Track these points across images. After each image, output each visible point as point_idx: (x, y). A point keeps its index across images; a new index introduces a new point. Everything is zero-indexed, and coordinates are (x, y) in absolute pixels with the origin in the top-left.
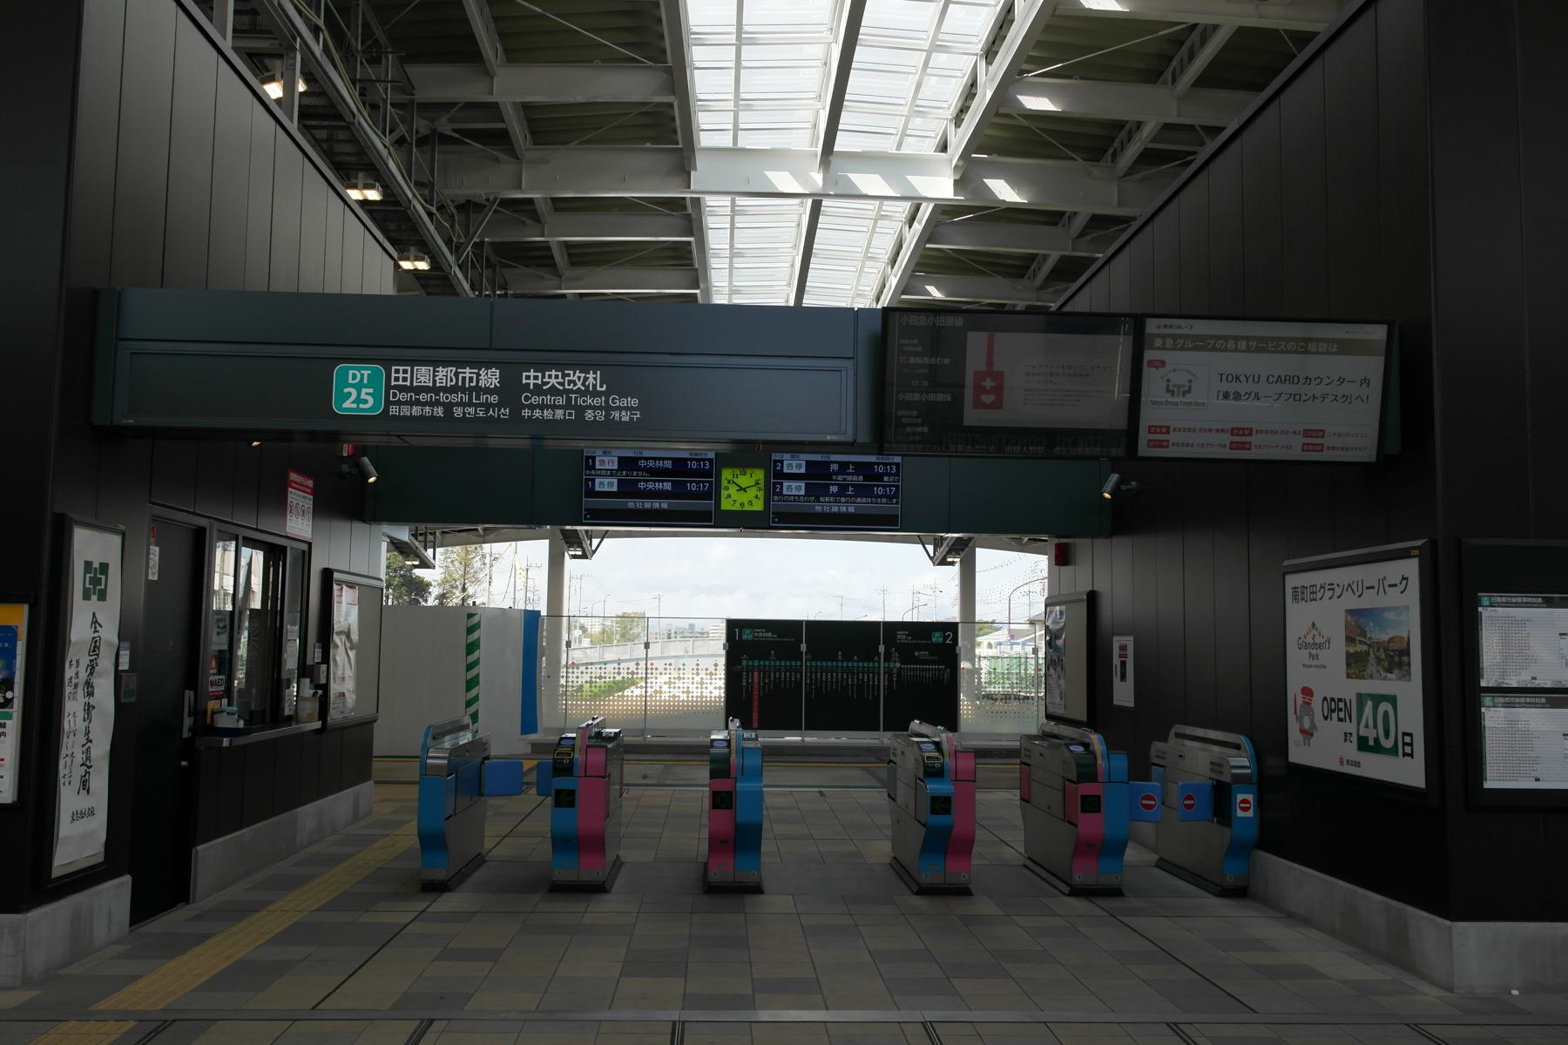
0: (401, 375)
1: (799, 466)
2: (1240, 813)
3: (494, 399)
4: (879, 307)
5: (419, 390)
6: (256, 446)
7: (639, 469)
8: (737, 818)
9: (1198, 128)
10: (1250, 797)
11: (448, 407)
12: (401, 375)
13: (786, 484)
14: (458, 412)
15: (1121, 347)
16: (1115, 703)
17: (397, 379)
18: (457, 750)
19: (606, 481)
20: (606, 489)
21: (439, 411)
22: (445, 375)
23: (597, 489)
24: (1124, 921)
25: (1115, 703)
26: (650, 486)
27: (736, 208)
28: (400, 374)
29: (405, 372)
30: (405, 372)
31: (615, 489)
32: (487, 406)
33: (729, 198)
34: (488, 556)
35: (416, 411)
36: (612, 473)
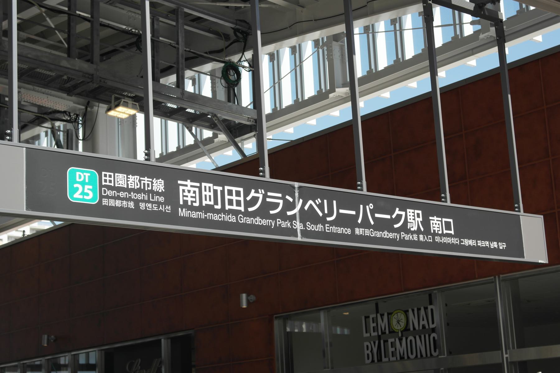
3: (162, 199)
5: (119, 189)
11: (137, 202)
14: (142, 206)
21: (131, 205)
32: (158, 203)
35: (118, 203)
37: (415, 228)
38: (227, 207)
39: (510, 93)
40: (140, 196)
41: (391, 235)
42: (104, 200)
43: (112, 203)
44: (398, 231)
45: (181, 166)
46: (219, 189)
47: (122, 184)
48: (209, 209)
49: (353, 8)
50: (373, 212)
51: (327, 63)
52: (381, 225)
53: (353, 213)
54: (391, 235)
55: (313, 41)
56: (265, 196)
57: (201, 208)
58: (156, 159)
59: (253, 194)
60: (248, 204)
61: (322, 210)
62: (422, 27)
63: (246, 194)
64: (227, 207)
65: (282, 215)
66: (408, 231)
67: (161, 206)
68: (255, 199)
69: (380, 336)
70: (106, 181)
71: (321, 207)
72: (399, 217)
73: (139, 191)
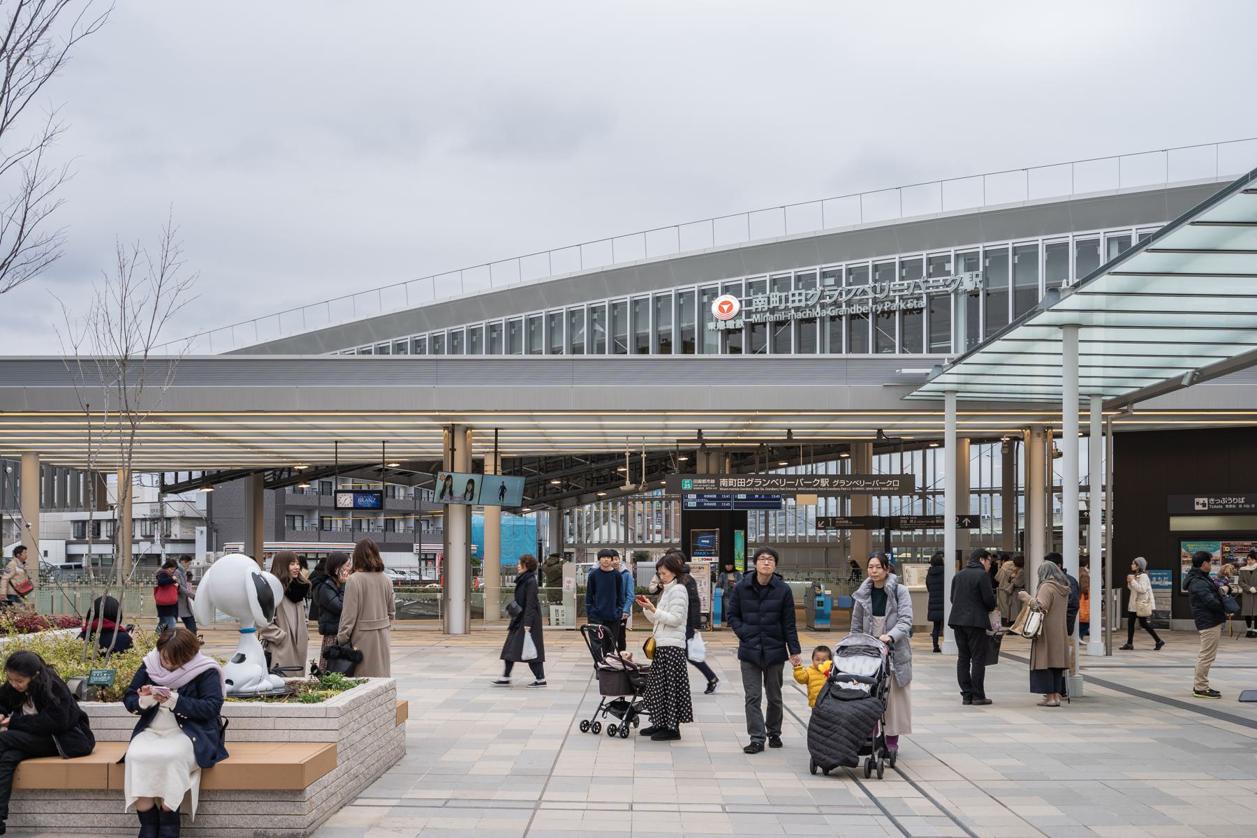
0: (741, 482)
1: (694, 504)
4: (1133, 562)
5: (699, 484)
7: (704, 498)
11: (705, 488)
12: (741, 482)
16: (1171, 529)
18: (672, 557)
19: (692, 503)
22: (704, 481)
25: (1171, 529)
26: (708, 504)
27: (866, 444)
28: (695, 481)
29: (740, 484)
30: (743, 481)
33: (998, 483)
34: (1069, 492)
36: (694, 500)
37: (824, 485)
40: (707, 485)
41: (814, 489)
42: (743, 481)
43: (697, 489)
44: (815, 487)
46: (735, 480)
47: (836, 275)
48: (732, 487)
49: (1134, 408)
50: (803, 482)
52: (881, 486)
54: (814, 489)
55: (483, 528)
56: (754, 481)
57: (728, 487)
59: (749, 480)
60: (746, 484)
62: (899, 454)
63: (746, 481)
65: (761, 486)
66: (821, 487)
67: (527, 629)
69: (986, 267)
70: (740, 481)
71: (778, 482)
73: (706, 484)
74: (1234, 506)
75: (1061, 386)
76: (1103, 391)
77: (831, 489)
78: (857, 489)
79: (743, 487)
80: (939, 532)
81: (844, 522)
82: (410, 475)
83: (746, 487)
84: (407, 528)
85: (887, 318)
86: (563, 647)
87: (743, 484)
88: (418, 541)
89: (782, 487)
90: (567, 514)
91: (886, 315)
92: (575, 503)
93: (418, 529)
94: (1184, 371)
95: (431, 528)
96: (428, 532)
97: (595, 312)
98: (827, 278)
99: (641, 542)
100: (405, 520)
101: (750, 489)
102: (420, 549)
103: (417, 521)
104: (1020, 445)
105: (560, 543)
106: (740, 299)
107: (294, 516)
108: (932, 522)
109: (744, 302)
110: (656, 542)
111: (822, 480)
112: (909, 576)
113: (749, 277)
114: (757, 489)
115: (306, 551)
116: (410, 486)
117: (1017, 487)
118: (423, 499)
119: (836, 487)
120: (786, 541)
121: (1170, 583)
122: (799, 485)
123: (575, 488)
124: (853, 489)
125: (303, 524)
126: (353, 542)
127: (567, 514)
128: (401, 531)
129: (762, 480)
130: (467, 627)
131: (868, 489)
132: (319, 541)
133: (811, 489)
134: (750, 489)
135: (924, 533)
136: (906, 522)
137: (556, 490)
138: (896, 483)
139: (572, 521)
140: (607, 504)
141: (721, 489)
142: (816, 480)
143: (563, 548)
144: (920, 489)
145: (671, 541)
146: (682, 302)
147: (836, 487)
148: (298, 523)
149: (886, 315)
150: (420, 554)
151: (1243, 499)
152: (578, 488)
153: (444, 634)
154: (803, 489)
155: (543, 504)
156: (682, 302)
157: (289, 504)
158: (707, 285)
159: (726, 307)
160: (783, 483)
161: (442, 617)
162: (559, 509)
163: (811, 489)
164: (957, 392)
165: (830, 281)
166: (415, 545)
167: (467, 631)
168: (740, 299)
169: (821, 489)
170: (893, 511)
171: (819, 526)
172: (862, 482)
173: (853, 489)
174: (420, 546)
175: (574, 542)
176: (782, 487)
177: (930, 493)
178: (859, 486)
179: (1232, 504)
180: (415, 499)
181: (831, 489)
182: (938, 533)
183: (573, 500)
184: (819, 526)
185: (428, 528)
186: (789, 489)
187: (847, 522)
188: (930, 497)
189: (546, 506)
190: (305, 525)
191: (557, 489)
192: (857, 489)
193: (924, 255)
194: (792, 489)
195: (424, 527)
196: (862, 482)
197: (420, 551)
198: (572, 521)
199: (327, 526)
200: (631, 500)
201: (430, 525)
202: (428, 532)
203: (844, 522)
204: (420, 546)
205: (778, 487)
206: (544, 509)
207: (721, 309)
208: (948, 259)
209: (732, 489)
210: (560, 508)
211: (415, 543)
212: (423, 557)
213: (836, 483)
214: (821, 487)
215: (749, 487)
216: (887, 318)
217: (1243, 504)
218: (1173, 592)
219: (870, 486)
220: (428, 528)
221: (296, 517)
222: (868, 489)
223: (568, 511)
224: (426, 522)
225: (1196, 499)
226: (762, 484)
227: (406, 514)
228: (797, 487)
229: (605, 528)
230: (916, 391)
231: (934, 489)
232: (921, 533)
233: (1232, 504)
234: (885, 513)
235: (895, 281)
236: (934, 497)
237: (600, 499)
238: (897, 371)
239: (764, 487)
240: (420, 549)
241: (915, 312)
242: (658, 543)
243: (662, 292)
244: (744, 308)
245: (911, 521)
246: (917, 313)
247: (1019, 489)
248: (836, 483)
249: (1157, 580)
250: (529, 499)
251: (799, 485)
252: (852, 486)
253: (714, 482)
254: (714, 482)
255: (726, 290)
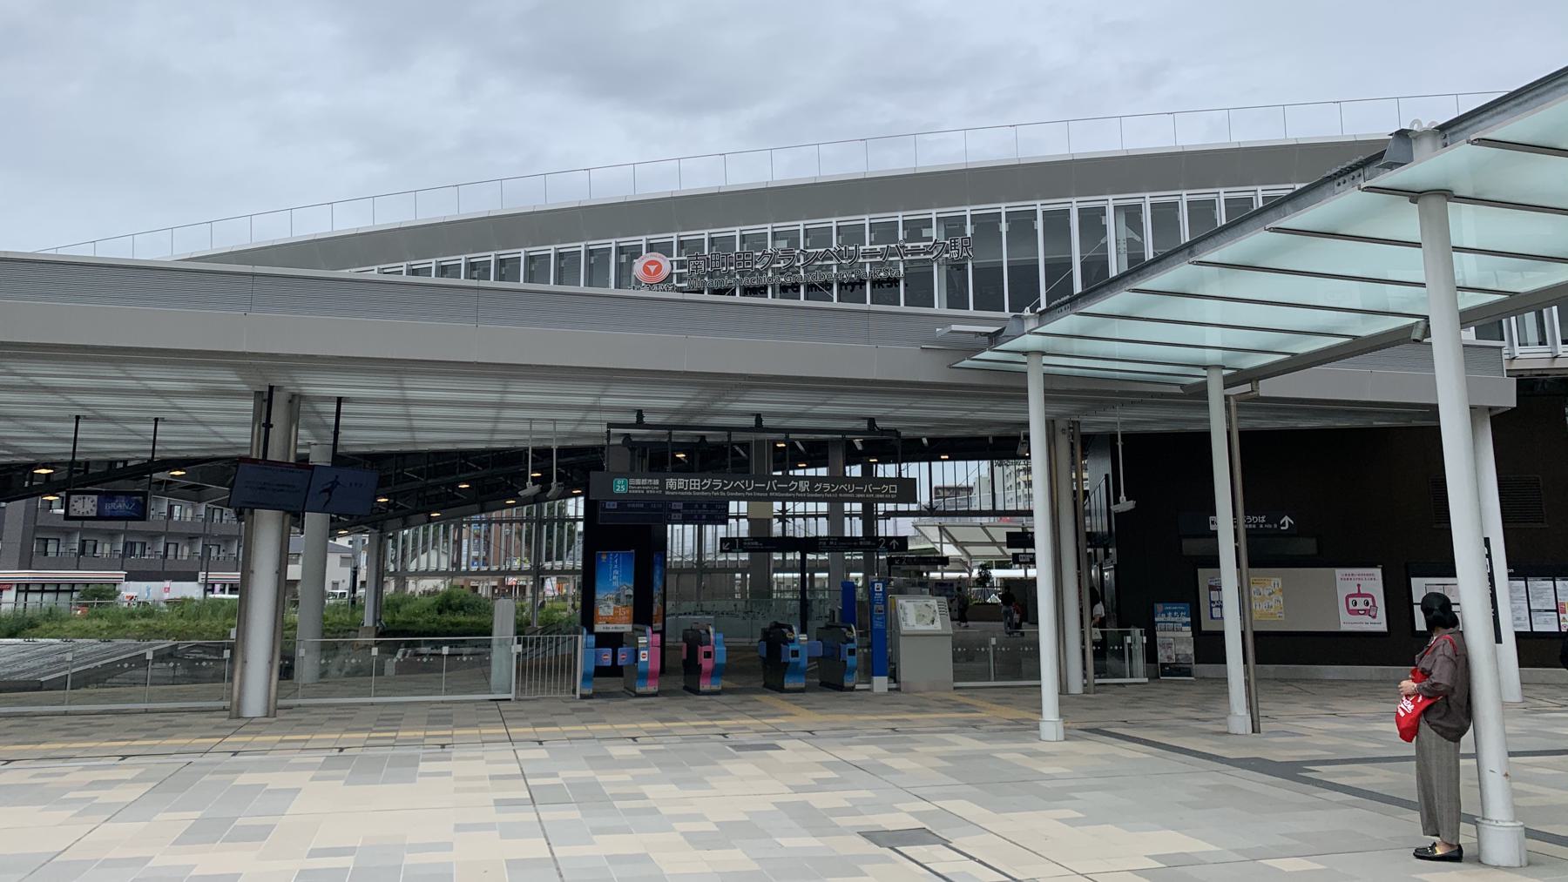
0: (695, 484)
2: (642, 659)
3: (657, 488)
5: (637, 486)
6: (24, 483)
8: (1516, 865)
9: (633, 278)
10: (642, 659)
11: (645, 490)
12: (695, 484)
13: (673, 515)
14: (648, 492)
15: (840, 436)
17: (693, 486)
20: (611, 507)
21: (643, 492)
22: (644, 481)
23: (607, 507)
24: (1004, 877)
28: (632, 481)
29: (697, 482)
30: (697, 482)
31: (616, 507)
32: (655, 490)
35: (636, 492)
38: (691, 488)
39: (502, 501)
41: (790, 495)
44: (793, 492)
45: (1307, 184)
47: (792, 238)
48: (681, 490)
50: (776, 485)
51: (89, 488)
52: (875, 492)
53: (763, 485)
56: (712, 482)
57: (677, 490)
58: (1129, 635)
59: (705, 481)
60: (702, 486)
61: (745, 486)
64: (691, 488)
65: (721, 489)
66: (800, 492)
68: (706, 484)
70: (693, 482)
71: (744, 484)
72: (885, 488)
74: (1254, 526)
75: (1423, 285)
76: (1223, 358)
77: (812, 495)
78: (845, 495)
79: (697, 491)
80: (1029, 550)
81: (753, 544)
82: (201, 488)
83: (701, 490)
84: (192, 553)
85: (852, 291)
86: (443, 746)
87: (697, 486)
88: (204, 569)
89: (748, 491)
90: (390, 537)
91: (849, 287)
92: (401, 524)
93: (206, 554)
94: (1413, 320)
95: (222, 554)
96: (218, 558)
97: (475, 270)
98: (778, 239)
99: (485, 568)
100: (191, 545)
101: (706, 494)
102: (207, 579)
103: (204, 546)
104: (878, 469)
105: (381, 571)
106: (671, 259)
107: (47, 540)
108: (855, 544)
109: (675, 264)
110: (513, 569)
111: (801, 482)
112: (905, 614)
113: (681, 234)
114: (715, 494)
115: (43, 581)
116: (199, 502)
117: (877, 511)
118: (215, 521)
119: (818, 493)
120: (737, 566)
121: (1189, 619)
122: (771, 489)
123: (402, 508)
124: (840, 495)
125: (58, 550)
126: (122, 570)
127: (390, 537)
128: (185, 558)
129: (722, 482)
130: (272, 701)
131: (859, 496)
132: (78, 569)
133: (787, 495)
134: (706, 494)
135: (784, 557)
136: (825, 543)
137: (381, 509)
138: (893, 489)
139: (395, 547)
140: (438, 526)
141: (667, 493)
142: (793, 482)
143: (383, 577)
144: (780, 511)
145: (499, 569)
146: (592, 262)
147: (818, 493)
148: (52, 548)
149: (849, 287)
150: (206, 584)
151: (1263, 518)
152: (406, 508)
153: (230, 718)
154: (777, 494)
155: (363, 526)
156: (592, 262)
157: (42, 524)
158: (627, 241)
159: (652, 268)
160: (750, 486)
161: (231, 679)
162: (381, 532)
163: (787, 495)
164: (1044, 354)
165: (783, 244)
166: (200, 573)
167: (272, 711)
168: (671, 259)
169: (799, 495)
170: (740, 533)
171: (724, 548)
172: (851, 487)
173: (840, 495)
174: (207, 575)
175: (396, 570)
176: (748, 491)
177: (789, 516)
178: (848, 492)
179: (1252, 523)
180: (205, 520)
181: (812, 495)
182: (820, 558)
183: (399, 522)
184: (724, 548)
185: (219, 553)
186: (758, 494)
187: (756, 543)
188: (790, 520)
189: (365, 528)
190: (62, 549)
191: (380, 509)
192: (845, 495)
193: (900, 217)
194: (761, 494)
195: (214, 553)
196: (851, 487)
197: (206, 581)
198: (395, 547)
199: (89, 550)
200: (466, 522)
201: (221, 550)
202: (218, 558)
203: (753, 544)
204: (207, 575)
205: (745, 491)
206: (364, 532)
207: (646, 269)
208: (927, 223)
209: (682, 493)
210: (382, 531)
211: (201, 571)
212: (209, 587)
213: (818, 487)
214: (800, 492)
215: (705, 491)
216: (852, 291)
217: (1264, 524)
218: (1192, 630)
219: (861, 492)
220: (219, 553)
221: (49, 541)
222: (859, 496)
223: (391, 534)
224: (217, 547)
225: (1211, 517)
226: (723, 486)
227: (192, 538)
228: (769, 492)
229: (423, 558)
230: (969, 359)
231: (794, 512)
232: (781, 558)
233: (1252, 523)
234: (800, 534)
235: (865, 245)
236: (794, 520)
237: (430, 520)
238: (938, 330)
239: (726, 491)
240: (207, 579)
241: (885, 285)
242: (443, 571)
243: (567, 247)
244: (675, 271)
245: (831, 543)
246: (888, 286)
247: (879, 513)
248: (818, 487)
249: (1173, 616)
250: (346, 520)
251: (771, 489)
252: (838, 492)
253: (658, 483)
254: (658, 483)
255: (651, 248)
